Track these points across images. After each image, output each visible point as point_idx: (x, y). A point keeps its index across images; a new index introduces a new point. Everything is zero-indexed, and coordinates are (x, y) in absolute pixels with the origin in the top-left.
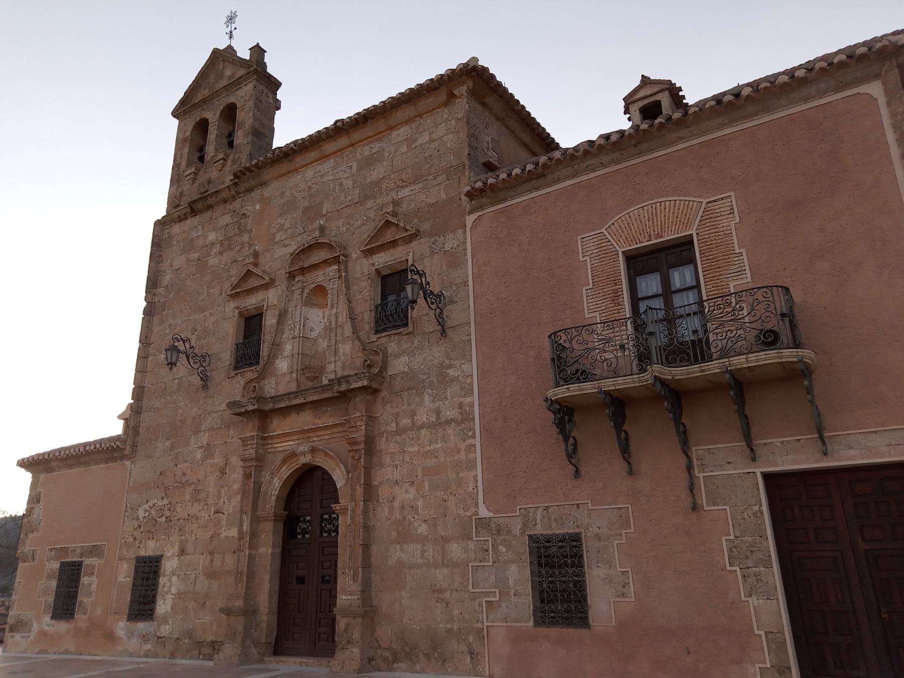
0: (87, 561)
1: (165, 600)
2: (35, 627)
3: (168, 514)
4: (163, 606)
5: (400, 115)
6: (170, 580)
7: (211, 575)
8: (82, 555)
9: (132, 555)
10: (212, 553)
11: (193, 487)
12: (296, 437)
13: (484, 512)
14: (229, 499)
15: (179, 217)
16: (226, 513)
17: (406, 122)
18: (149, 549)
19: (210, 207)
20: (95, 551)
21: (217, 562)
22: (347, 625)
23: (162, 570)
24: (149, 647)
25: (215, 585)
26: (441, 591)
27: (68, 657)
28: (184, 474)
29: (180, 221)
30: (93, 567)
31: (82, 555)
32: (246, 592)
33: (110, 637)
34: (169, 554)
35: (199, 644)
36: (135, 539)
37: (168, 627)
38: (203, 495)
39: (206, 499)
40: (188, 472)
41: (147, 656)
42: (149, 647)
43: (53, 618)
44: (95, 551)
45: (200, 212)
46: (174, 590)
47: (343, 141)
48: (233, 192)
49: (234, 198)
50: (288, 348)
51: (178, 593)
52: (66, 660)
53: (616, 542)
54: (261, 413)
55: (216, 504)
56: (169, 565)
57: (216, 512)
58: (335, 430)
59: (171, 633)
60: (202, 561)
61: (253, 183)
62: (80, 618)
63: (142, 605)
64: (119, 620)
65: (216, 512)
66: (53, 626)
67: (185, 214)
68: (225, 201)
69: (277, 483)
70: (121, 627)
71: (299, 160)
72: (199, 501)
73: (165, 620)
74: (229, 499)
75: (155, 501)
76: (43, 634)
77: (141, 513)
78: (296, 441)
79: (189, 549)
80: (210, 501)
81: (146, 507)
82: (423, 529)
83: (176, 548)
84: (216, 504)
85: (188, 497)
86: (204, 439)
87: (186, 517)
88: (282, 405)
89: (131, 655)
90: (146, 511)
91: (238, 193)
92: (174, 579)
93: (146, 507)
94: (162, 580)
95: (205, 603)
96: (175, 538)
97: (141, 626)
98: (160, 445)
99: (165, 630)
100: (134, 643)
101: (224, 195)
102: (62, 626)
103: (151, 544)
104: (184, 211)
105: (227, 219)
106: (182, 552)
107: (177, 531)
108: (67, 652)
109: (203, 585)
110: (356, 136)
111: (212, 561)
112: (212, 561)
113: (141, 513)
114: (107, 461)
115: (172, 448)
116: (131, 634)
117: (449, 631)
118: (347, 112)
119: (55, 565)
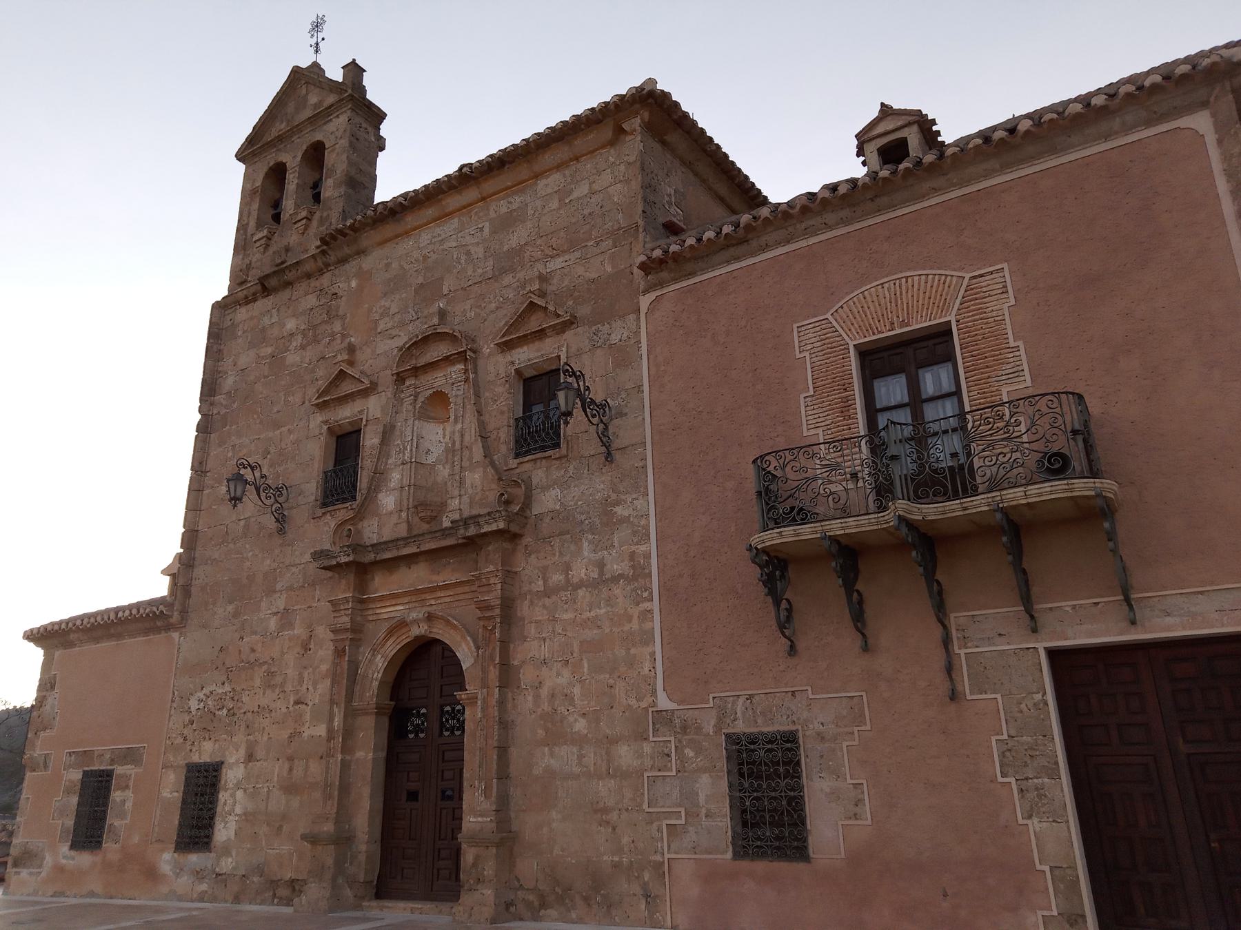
0: (120, 770)
1: (226, 823)
2: (49, 860)
4: (224, 832)
5: (549, 158)
6: (233, 796)
7: (290, 788)
8: (112, 761)
9: (181, 761)
10: (290, 759)
13: (664, 703)
14: (315, 684)
15: (246, 297)
16: (311, 704)
17: (558, 167)
18: (205, 753)
19: (289, 284)
20: (130, 756)
21: (298, 772)
22: (477, 858)
23: (223, 782)
24: (204, 887)
25: (295, 802)
26: (606, 810)
27: (94, 901)
28: (253, 650)
30: (128, 777)
31: (112, 761)
33: (152, 874)
34: (232, 760)
35: (274, 884)
36: (185, 739)
37: (230, 860)
38: (278, 679)
39: (282, 685)
40: (259, 648)
42: (204, 887)
43: (72, 847)
44: (130, 756)
46: (238, 810)
47: (471, 194)
48: (320, 263)
49: (321, 272)
51: (245, 814)
52: (90, 905)
54: (359, 567)
55: (297, 692)
56: (232, 775)
57: (297, 703)
58: (460, 590)
60: (278, 769)
61: (347, 250)
62: (110, 848)
63: (195, 830)
64: (163, 851)
65: (297, 703)
67: (254, 294)
68: (309, 276)
69: (380, 662)
70: (166, 860)
71: (410, 220)
73: (226, 851)
74: (315, 684)
75: (213, 687)
77: (194, 704)
78: (406, 605)
79: (260, 753)
81: (201, 695)
82: (581, 725)
83: (242, 752)
84: (297, 692)
85: (258, 682)
86: (280, 603)
87: (256, 709)
88: (388, 555)
90: (200, 701)
91: (327, 265)
92: (239, 794)
94: (223, 796)
95: (281, 826)
96: (240, 737)
97: (194, 859)
99: (227, 865)
100: (184, 883)
101: (308, 267)
102: (85, 859)
103: (208, 746)
104: (252, 290)
105: (311, 301)
106: (250, 757)
108: (92, 894)
109: (278, 802)
110: (489, 186)
112: (291, 769)
113: (194, 704)
114: (147, 632)
115: (236, 615)
116: (179, 870)
117: (616, 866)
118: (476, 153)
119: (76, 775)
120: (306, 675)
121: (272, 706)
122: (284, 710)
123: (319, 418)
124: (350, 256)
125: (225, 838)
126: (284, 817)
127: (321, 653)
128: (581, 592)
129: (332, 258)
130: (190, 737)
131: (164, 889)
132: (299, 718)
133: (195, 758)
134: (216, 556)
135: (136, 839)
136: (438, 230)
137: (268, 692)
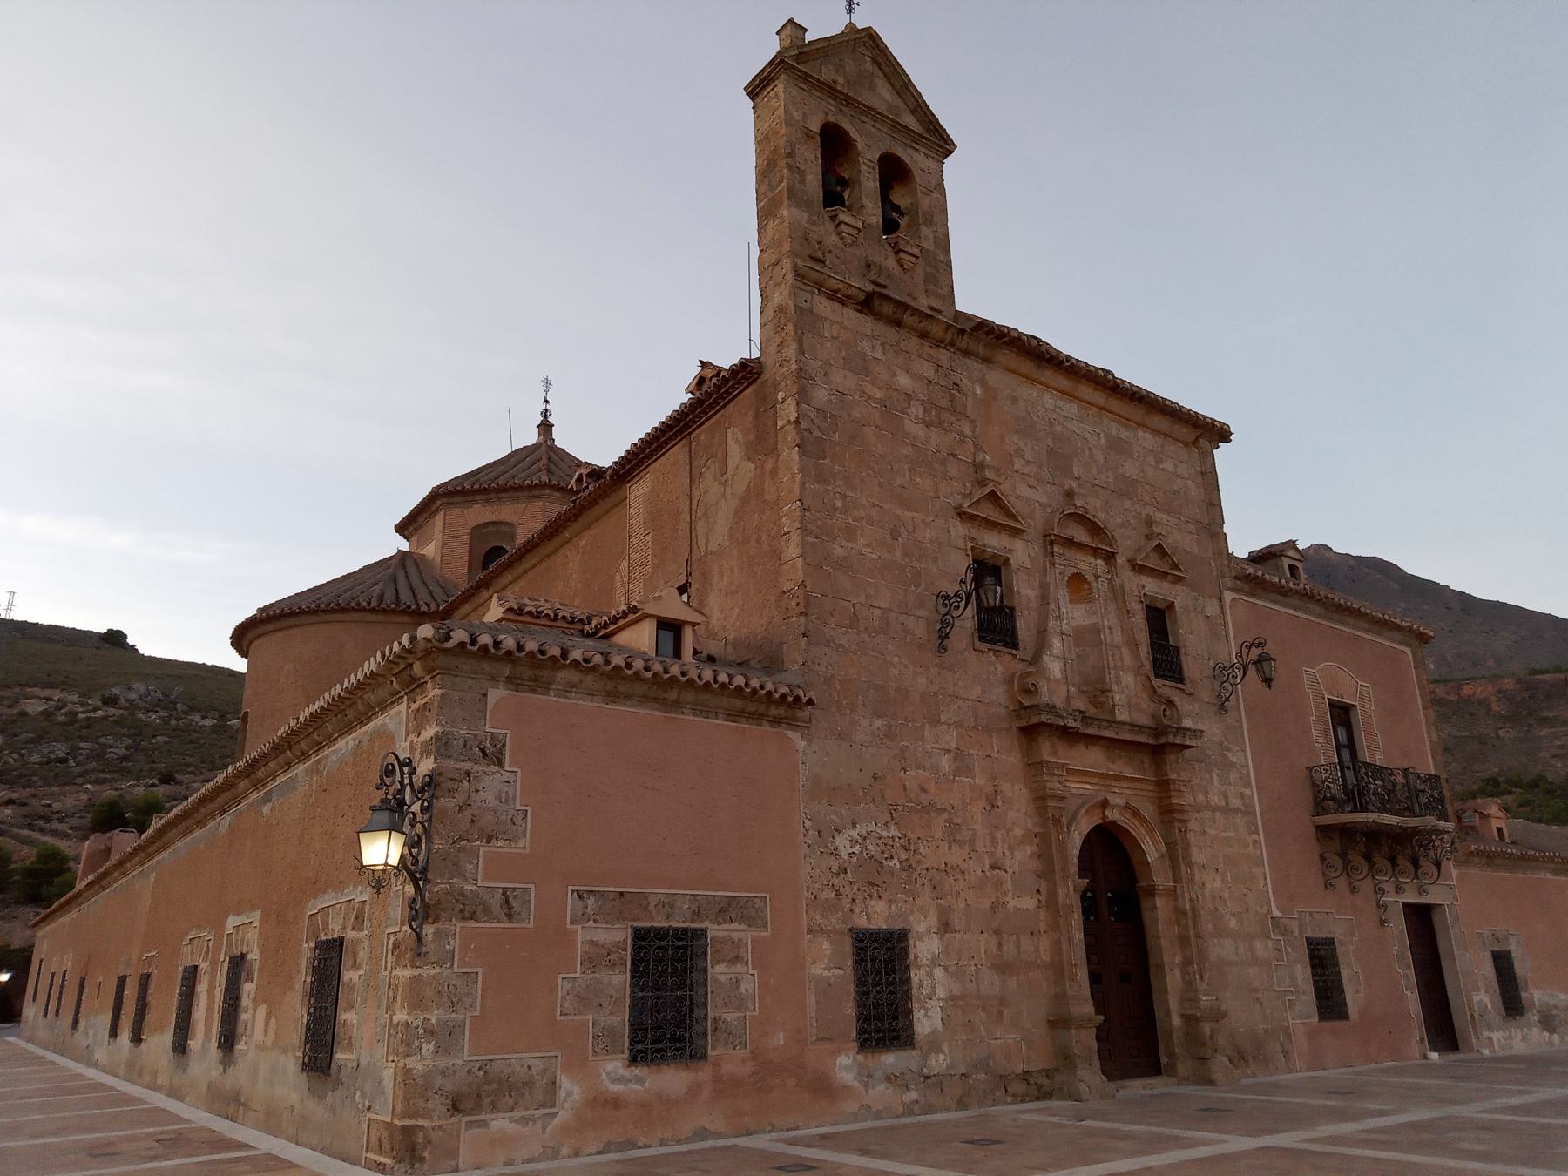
0: (715, 930)
1: (926, 1010)
2: (571, 1089)
3: (903, 856)
4: (926, 1021)
5: (1158, 421)
6: (930, 975)
7: (1003, 967)
8: (696, 915)
9: (834, 921)
10: (997, 932)
11: (945, 816)
12: (1095, 780)
13: (1276, 913)
14: (1012, 849)
15: (836, 291)
16: (1010, 871)
17: (1155, 432)
18: (878, 915)
19: (898, 323)
20: (727, 909)
21: (1009, 948)
22: (1212, 1030)
23: (912, 957)
24: (913, 1095)
25: (1012, 983)
26: (1255, 990)
27: (709, 1144)
28: (924, 790)
29: (830, 297)
30: (739, 944)
31: (696, 915)
32: (1497, 970)
33: (823, 1088)
34: (921, 928)
35: (1003, 1081)
36: (838, 894)
37: (942, 1057)
38: (964, 834)
39: (972, 842)
40: (931, 786)
41: (911, 1113)
42: (913, 1095)
43: (633, 1060)
44: (727, 909)
45: (878, 316)
46: (941, 993)
47: (1099, 398)
48: (949, 337)
49: (938, 343)
50: (1057, 645)
51: (952, 998)
52: (715, 1149)
53: (480, 971)
54: (1034, 727)
55: (992, 854)
56: (924, 948)
57: (993, 867)
58: (1138, 785)
59: (951, 1066)
60: (983, 944)
61: (981, 349)
62: (728, 1059)
63: (883, 1017)
64: (838, 1052)
65: (993, 867)
66: (640, 1081)
67: (849, 297)
68: (924, 335)
69: (1078, 842)
70: (845, 1065)
71: (1048, 375)
72: (961, 844)
73: (934, 1045)
74: (1012, 849)
75: (872, 827)
76: (605, 1105)
77: (842, 843)
78: (1095, 785)
79: (957, 923)
80: (980, 847)
81: (854, 833)
82: (1233, 923)
83: (933, 920)
84: (992, 854)
85: (938, 834)
86: (951, 739)
87: (942, 867)
88: (1090, 731)
89: (878, 1116)
90: (853, 842)
91: (952, 344)
92: (939, 973)
93: (854, 833)
94: (915, 976)
95: (1000, 1013)
96: (926, 898)
97: (890, 1060)
98: (865, 723)
99: (938, 1063)
100: (881, 1093)
101: (936, 330)
102: (672, 1079)
103: (879, 907)
104: (852, 292)
105: (928, 371)
106: (945, 927)
107: (927, 889)
108: (703, 1133)
109: (990, 983)
110: (1114, 404)
111: (1000, 945)
112: (1000, 945)
113: (842, 843)
114: (734, 715)
115: (890, 734)
116: (867, 1076)
117: (1266, 1031)
118: (1127, 373)
119: (618, 935)
120: (998, 835)
121: (964, 866)
122: (979, 872)
123: (959, 530)
124: (977, 356)
125: (928, 1030)
126: (1002, 1001)
127: (1012, 814)
128: (1218, 814)
129: (964, 343)
130: (846, 890)
131: (851, 1107)
132: (999, 883)
133: (862, 922)
134: (844, 641)
135: (780, 1039)
136: (1060, 403)
137: (955, 847)
